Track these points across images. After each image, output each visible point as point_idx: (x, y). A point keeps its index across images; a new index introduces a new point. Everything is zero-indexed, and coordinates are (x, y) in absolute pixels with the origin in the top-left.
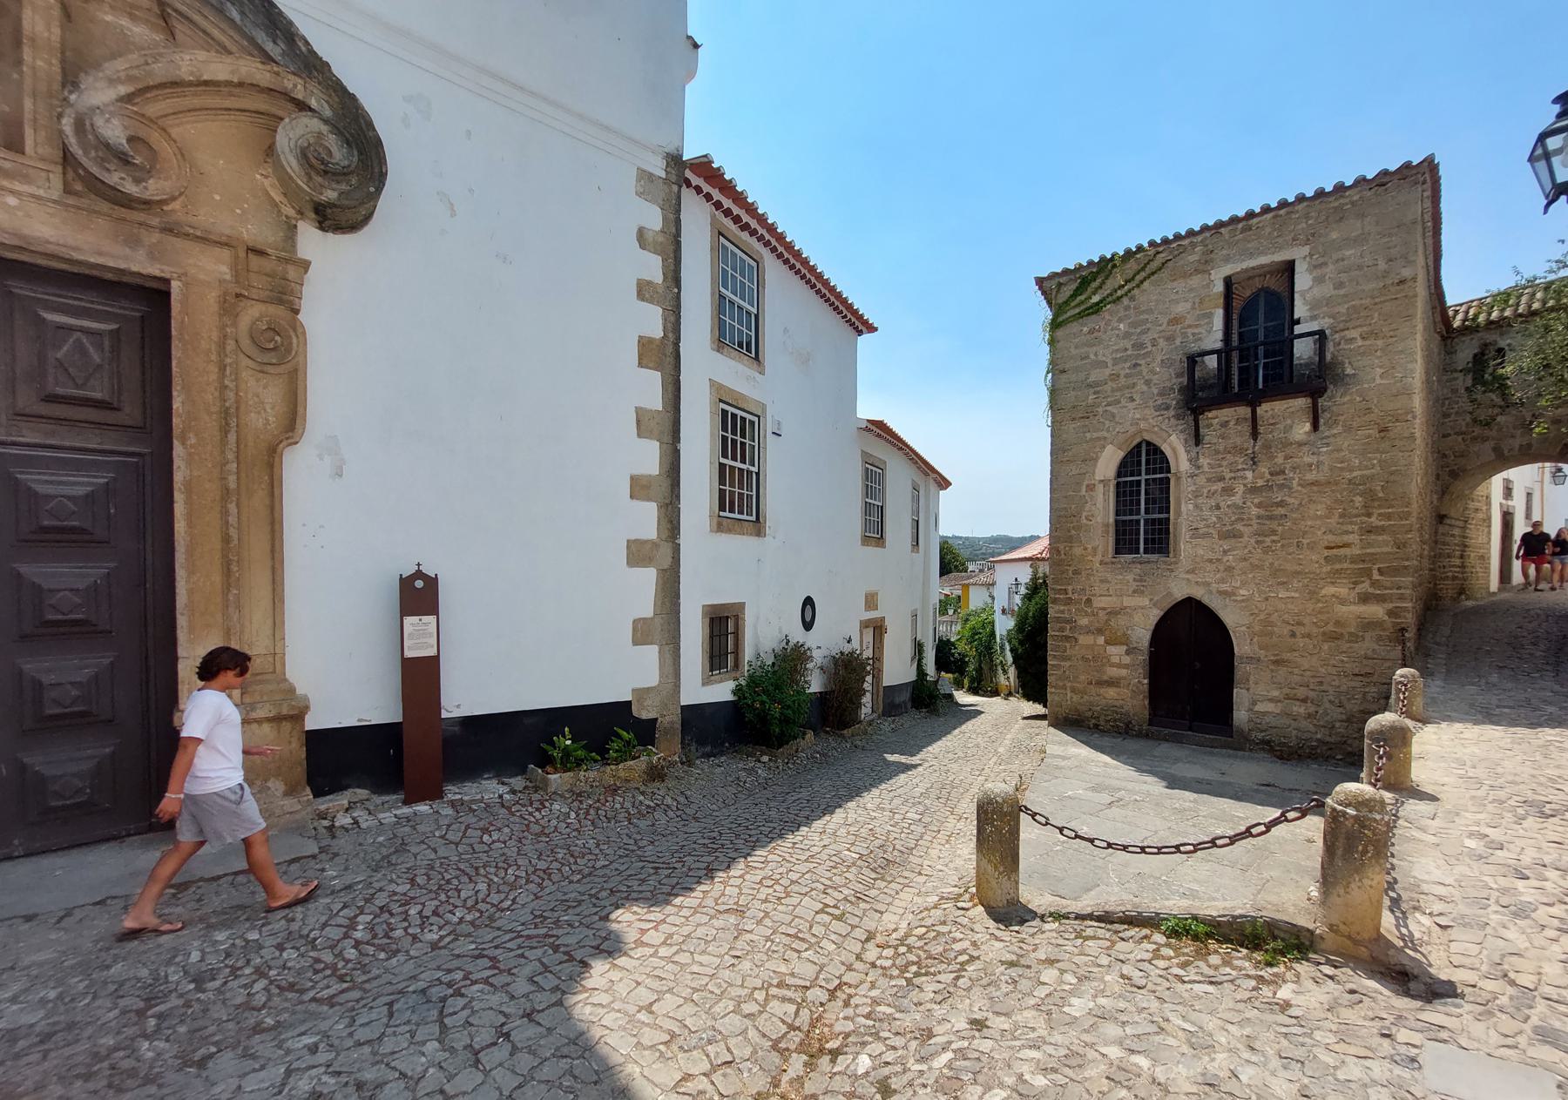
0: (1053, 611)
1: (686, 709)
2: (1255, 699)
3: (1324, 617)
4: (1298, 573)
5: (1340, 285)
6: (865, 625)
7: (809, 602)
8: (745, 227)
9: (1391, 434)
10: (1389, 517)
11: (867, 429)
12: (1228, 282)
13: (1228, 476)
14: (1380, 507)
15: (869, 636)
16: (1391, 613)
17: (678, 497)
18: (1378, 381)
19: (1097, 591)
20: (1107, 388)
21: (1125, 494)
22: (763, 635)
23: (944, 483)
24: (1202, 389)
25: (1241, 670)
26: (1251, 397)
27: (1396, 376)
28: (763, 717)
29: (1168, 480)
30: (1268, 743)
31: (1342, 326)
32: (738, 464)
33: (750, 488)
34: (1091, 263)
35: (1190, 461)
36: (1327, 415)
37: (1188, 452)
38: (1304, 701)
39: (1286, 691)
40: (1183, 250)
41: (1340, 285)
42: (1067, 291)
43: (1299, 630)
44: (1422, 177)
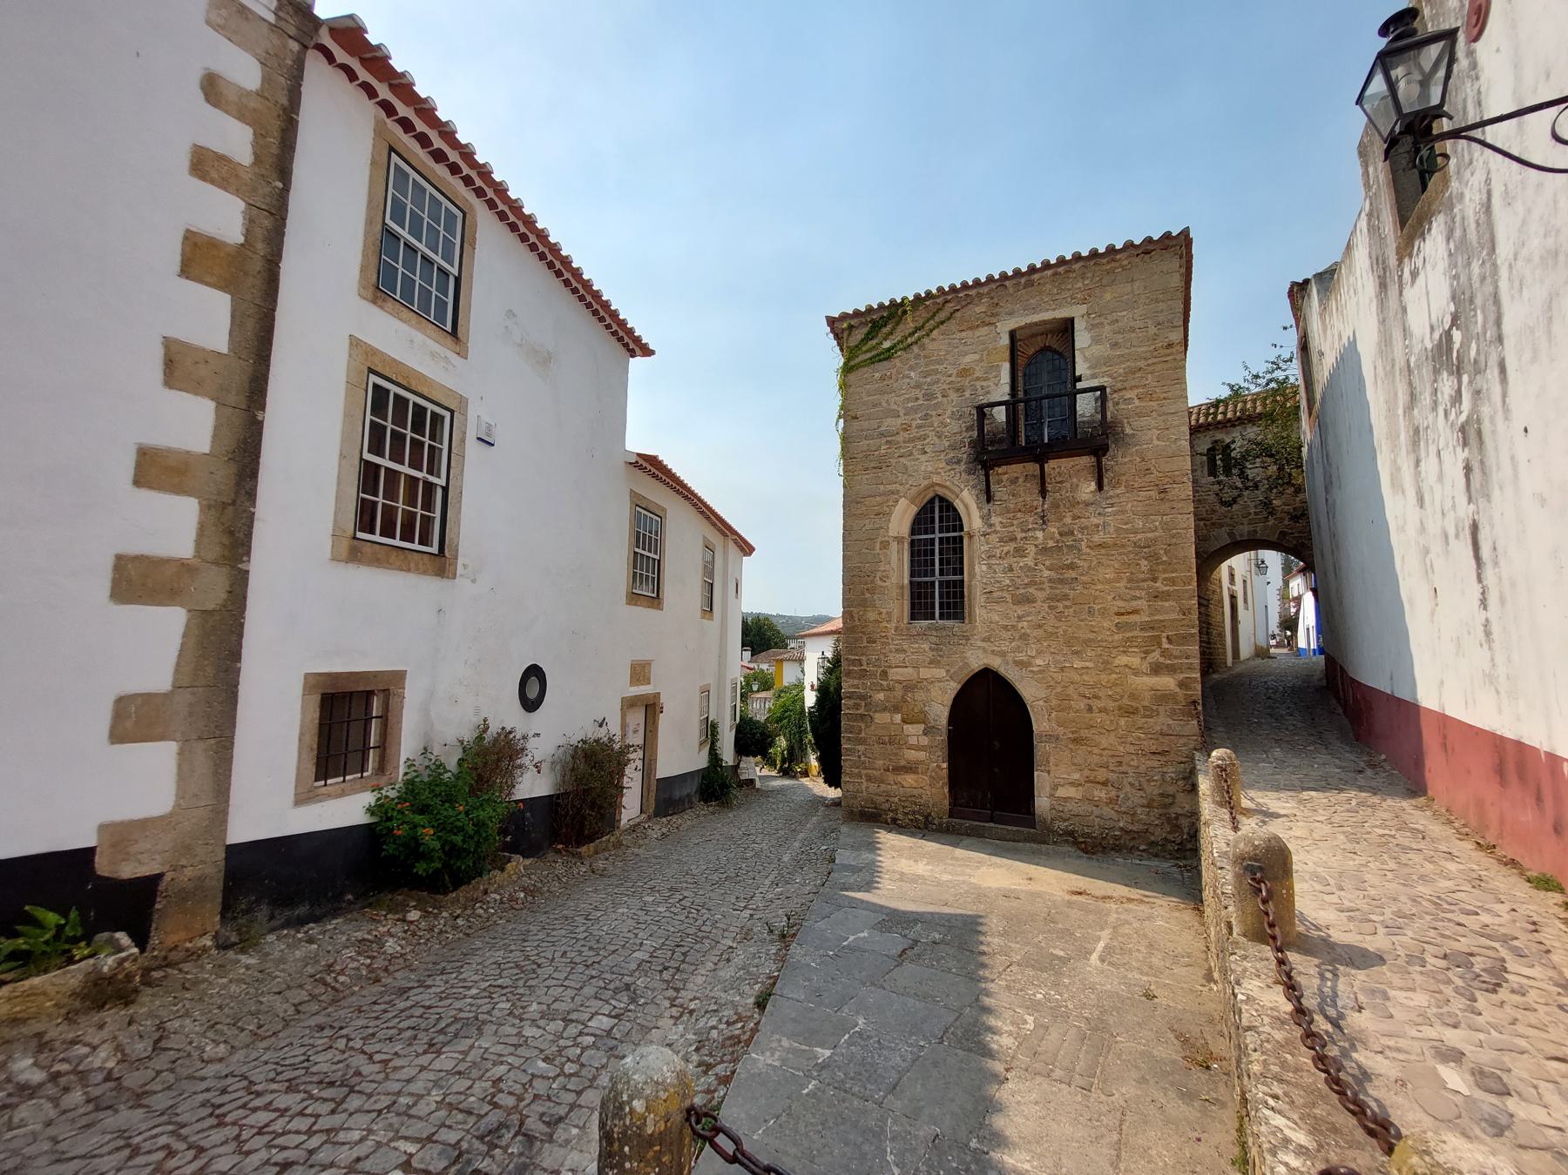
0: (846, 688)
1: (234, 851)
2: (1056, 786)
3: (1118, 689)
4: (1090, 640)
5: (1115, 345)
6: (629, 704)
7: (534, 673)
8: (439, 156)
9: (1169, 496)
10: (1173, 581)
11: (635, 465)
12: (1012, 334)
13: (1020, 535)
14: (1165, 571)
15: (637, 718)
16: (1181, 684)
17: (252, 495)
18: (1156, 442)
19: (895, 658)
20: (900, 438)
21: (920, 555)
22: (434, 721)
23: (746, 549)
24: (992, 443)
25: (1041, 749)
26: (1039, 453)
27: (1159, 449)
28: (414, 848)
29: (961, 538)
30: (1071, 833)
31: (1119, 385)
32: (405, 469)
33: (428, 505)
34: (881, 306)
35: (982, 518)
36: (1110, 474)
37: (980, 509)
38: (1105, 784)
39: (1086, 772)
40: (969, 301)
41: (1115, 345)
42: (859, 335)
43: (1096, 704)
44: (1177, 246)
